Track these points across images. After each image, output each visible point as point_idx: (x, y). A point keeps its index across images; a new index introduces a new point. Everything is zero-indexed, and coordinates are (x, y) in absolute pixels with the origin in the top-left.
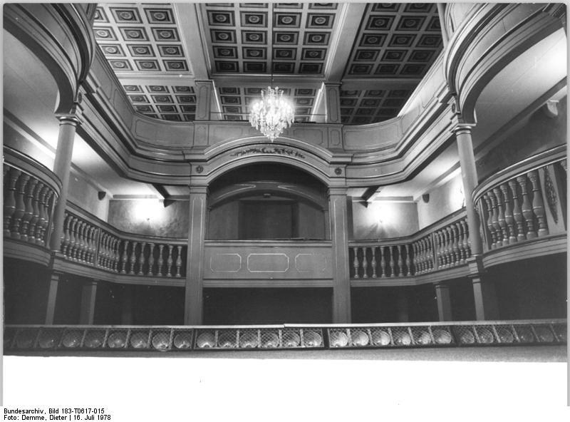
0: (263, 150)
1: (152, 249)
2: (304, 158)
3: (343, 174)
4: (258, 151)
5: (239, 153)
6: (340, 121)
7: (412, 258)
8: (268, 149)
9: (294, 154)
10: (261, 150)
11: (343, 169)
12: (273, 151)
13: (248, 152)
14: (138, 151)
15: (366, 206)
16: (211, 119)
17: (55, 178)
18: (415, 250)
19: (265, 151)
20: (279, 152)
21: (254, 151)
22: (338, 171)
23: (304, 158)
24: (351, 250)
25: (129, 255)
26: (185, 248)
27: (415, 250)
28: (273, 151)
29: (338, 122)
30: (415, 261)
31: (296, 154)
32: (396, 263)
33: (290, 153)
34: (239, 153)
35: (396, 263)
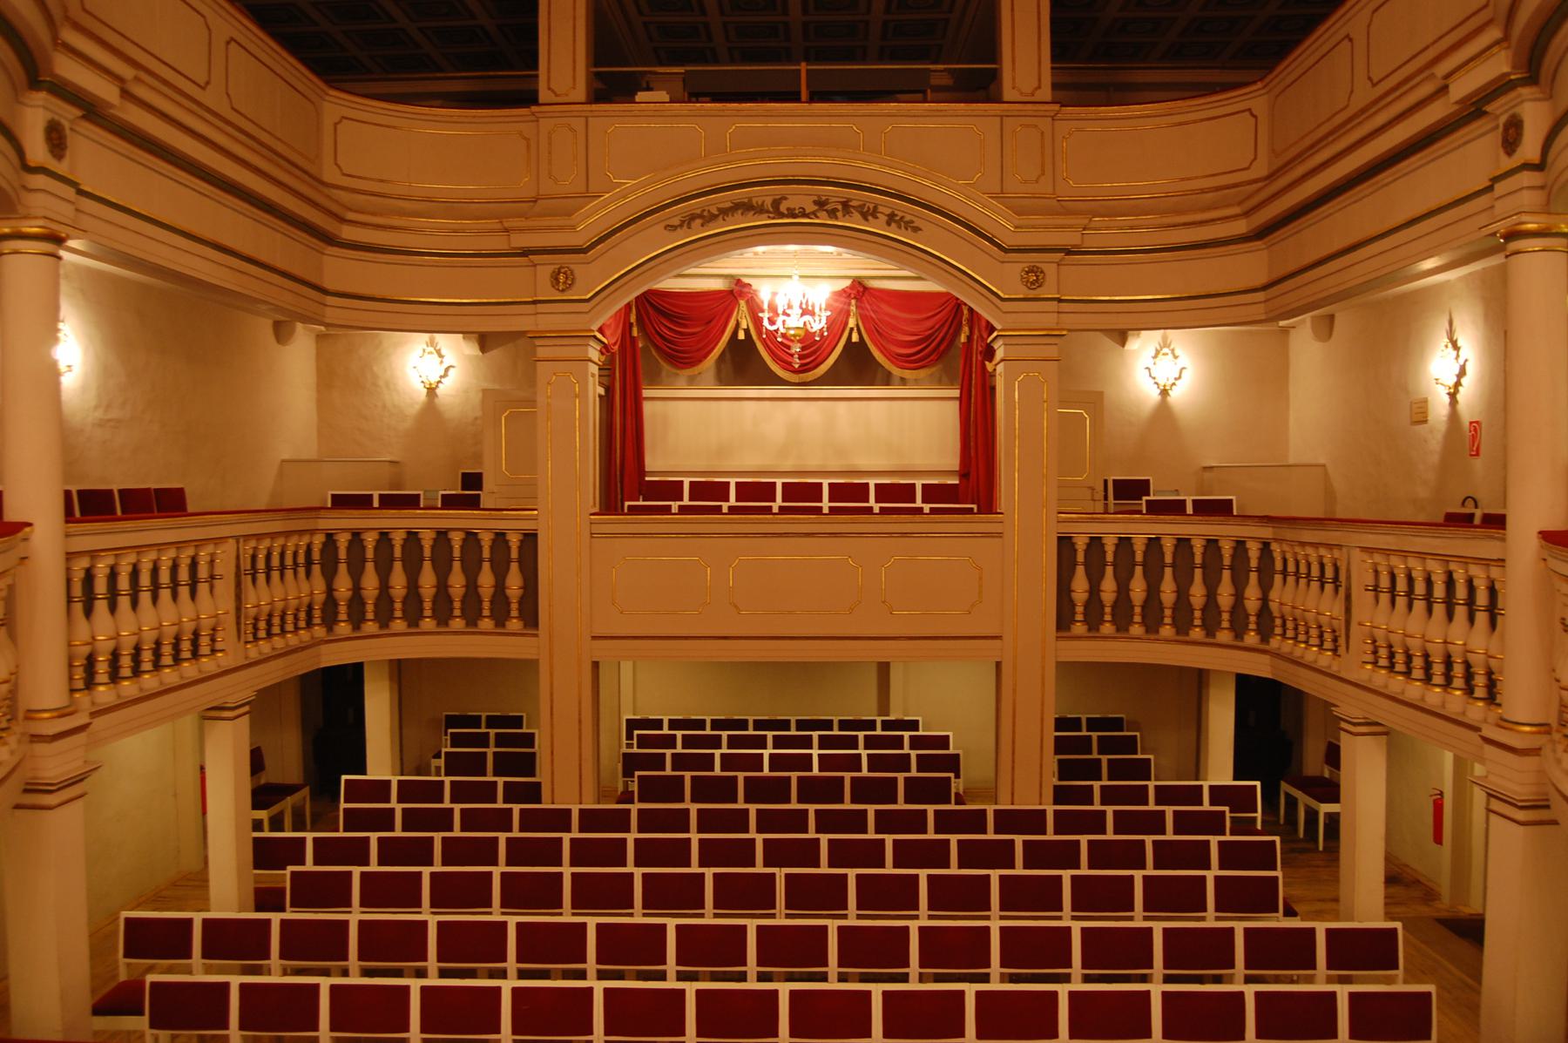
0: (776, 203)
1: (427, 545)
2: (916, 229)
3: (1047, 291)
4: (760, 210)
5: (693, 218)
6: (1046, 93)
7: (1266, 586)
8: (792, 203)
9: (883, 218)
10: (768, 201)
11: (1051, 270)
12: (810, 208)
13: (724, 212)
14: (348, 233)
15: (1123, 345)
16: (659, 461)
17: (213, 714)
18: (1279, 566)
19: (783, 208)
20: (832, 214)
21: (747, 207)
22: (1034, 277)
23: (916, 229)
24: (1065, 543)
25: (356, 574)
26: (530, 539)
27: (1279, 566)
28: (810, 208)
29: (1038, 97)
30: (1274, 595)
31: (891, 219)
32: (1211, 595)
33: (868, 213)
34: (693, 218)
35: (1211, 595)
